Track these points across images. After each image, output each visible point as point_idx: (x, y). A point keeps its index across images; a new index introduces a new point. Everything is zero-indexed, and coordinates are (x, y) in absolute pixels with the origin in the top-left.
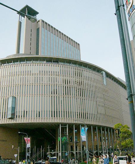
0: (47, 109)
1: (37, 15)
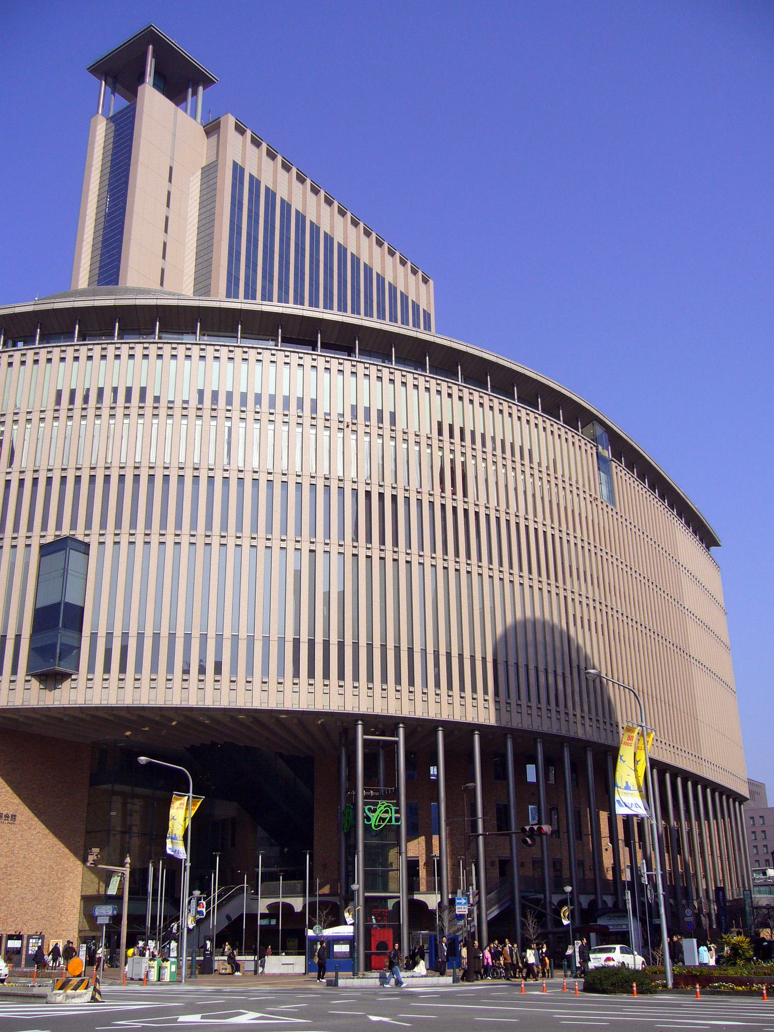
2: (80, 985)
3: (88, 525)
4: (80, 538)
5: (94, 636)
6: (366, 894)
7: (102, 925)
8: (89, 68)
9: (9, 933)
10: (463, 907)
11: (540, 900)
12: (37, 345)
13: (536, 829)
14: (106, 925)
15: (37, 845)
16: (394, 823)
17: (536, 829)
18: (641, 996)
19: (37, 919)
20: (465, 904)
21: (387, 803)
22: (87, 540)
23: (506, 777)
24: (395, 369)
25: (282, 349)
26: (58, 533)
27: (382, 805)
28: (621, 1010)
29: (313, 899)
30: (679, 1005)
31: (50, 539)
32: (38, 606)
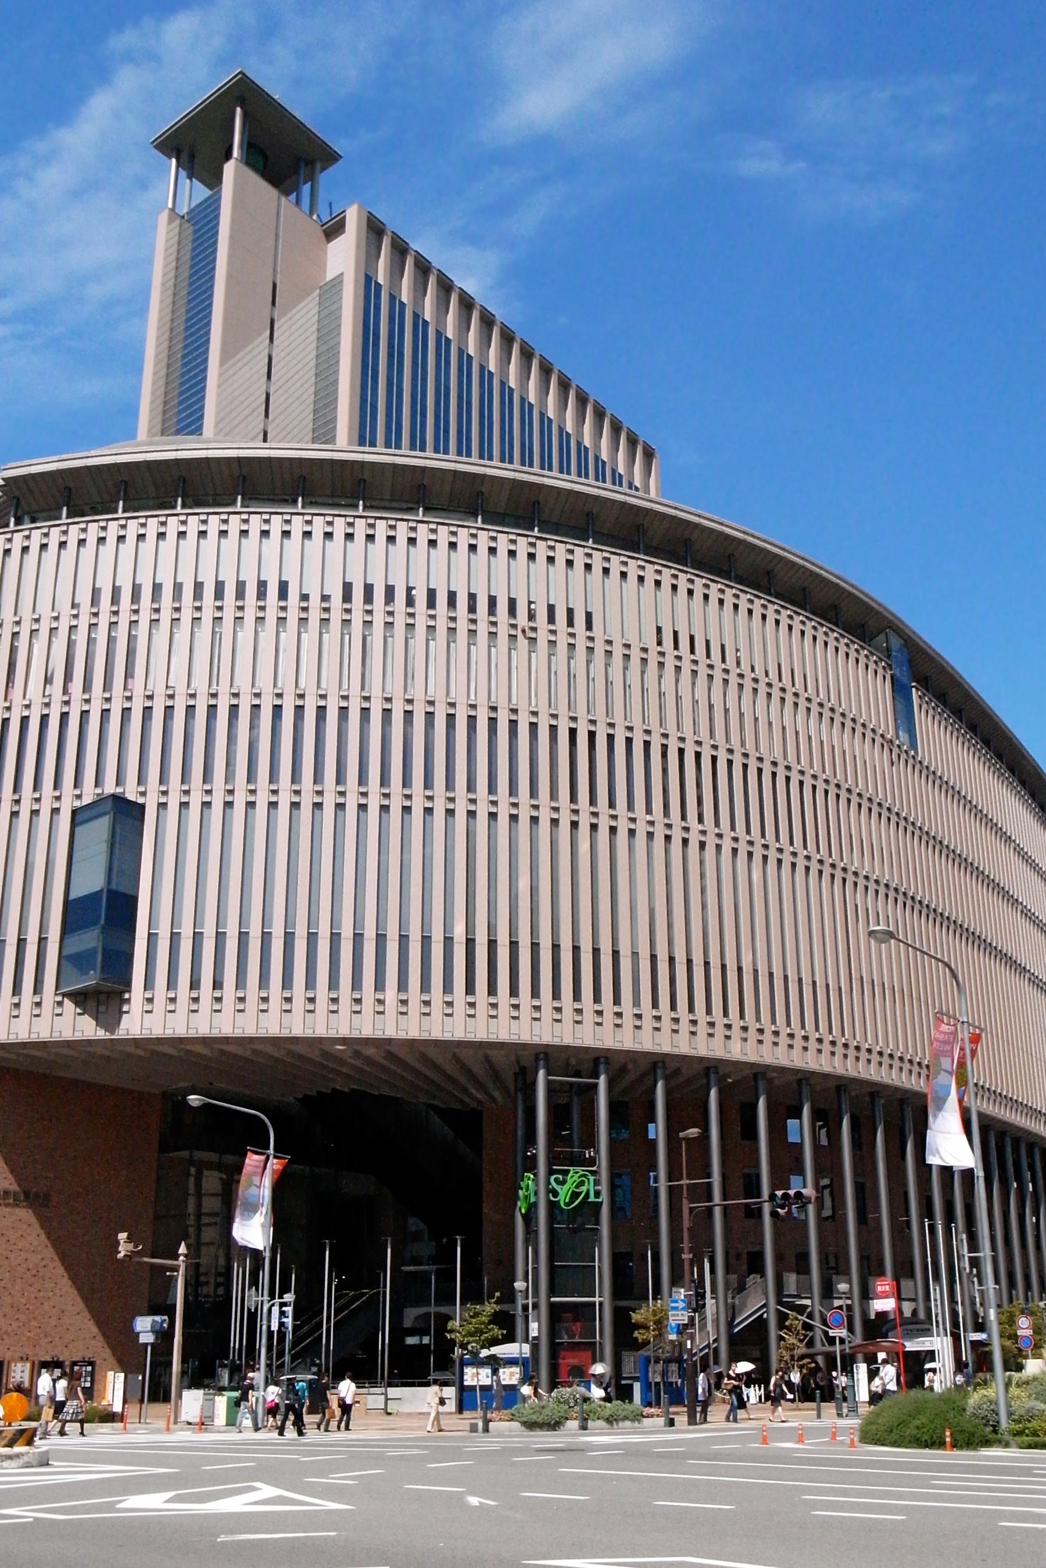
0: (312, 919)
1: (326, 178)
2: (18, 1439)
3: (141, 780)
4: (131, 796)
5: (152, 938)
6: (552, 1299)
7: (146, 1345)
8: (154, 142)
9: (43, 1359)
10: (680, 1313)
11: (807, 1306)
12: (64, 521)
13: (792, 1195)
14: (152, 1344)
15: (84, 1235)
16: (592, 1199)
17: (792, 1195)
18: (956, 1452)
19: (84, 1339)
20: (683, 1309)
21: (583, 1171)
22: (141, 800)
23: (754, 1136)
24: (593, 549)
25: (425, 519)
26: (99, 791)
27: (575, 1174)
28: (924, 1483)
29: (843, 1347)
30: (1028, 1472)
31: (87, 800)
32: (73, 896)
